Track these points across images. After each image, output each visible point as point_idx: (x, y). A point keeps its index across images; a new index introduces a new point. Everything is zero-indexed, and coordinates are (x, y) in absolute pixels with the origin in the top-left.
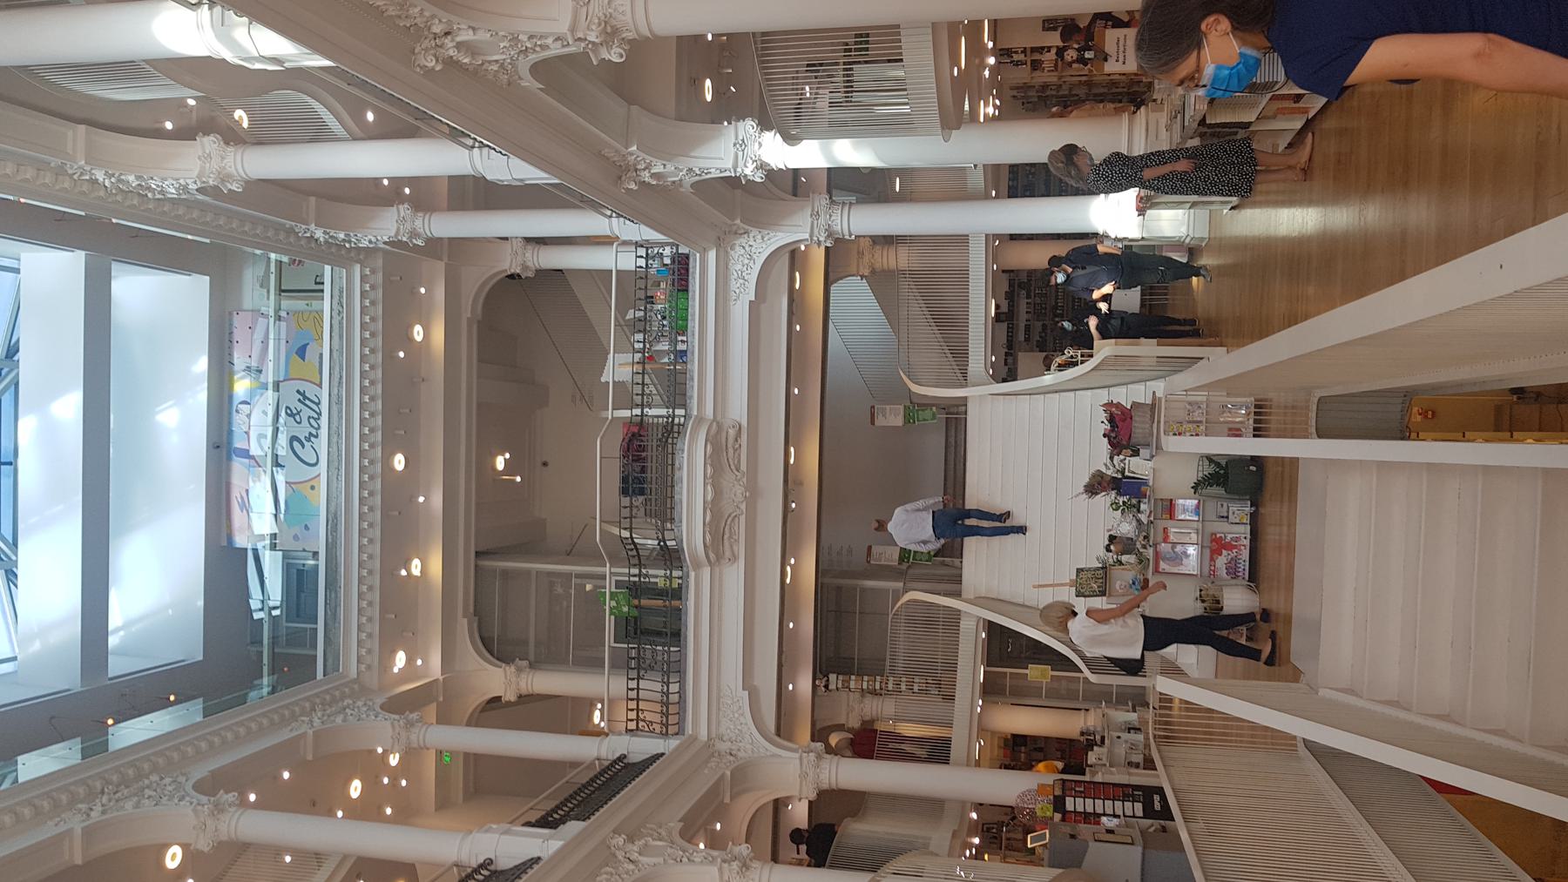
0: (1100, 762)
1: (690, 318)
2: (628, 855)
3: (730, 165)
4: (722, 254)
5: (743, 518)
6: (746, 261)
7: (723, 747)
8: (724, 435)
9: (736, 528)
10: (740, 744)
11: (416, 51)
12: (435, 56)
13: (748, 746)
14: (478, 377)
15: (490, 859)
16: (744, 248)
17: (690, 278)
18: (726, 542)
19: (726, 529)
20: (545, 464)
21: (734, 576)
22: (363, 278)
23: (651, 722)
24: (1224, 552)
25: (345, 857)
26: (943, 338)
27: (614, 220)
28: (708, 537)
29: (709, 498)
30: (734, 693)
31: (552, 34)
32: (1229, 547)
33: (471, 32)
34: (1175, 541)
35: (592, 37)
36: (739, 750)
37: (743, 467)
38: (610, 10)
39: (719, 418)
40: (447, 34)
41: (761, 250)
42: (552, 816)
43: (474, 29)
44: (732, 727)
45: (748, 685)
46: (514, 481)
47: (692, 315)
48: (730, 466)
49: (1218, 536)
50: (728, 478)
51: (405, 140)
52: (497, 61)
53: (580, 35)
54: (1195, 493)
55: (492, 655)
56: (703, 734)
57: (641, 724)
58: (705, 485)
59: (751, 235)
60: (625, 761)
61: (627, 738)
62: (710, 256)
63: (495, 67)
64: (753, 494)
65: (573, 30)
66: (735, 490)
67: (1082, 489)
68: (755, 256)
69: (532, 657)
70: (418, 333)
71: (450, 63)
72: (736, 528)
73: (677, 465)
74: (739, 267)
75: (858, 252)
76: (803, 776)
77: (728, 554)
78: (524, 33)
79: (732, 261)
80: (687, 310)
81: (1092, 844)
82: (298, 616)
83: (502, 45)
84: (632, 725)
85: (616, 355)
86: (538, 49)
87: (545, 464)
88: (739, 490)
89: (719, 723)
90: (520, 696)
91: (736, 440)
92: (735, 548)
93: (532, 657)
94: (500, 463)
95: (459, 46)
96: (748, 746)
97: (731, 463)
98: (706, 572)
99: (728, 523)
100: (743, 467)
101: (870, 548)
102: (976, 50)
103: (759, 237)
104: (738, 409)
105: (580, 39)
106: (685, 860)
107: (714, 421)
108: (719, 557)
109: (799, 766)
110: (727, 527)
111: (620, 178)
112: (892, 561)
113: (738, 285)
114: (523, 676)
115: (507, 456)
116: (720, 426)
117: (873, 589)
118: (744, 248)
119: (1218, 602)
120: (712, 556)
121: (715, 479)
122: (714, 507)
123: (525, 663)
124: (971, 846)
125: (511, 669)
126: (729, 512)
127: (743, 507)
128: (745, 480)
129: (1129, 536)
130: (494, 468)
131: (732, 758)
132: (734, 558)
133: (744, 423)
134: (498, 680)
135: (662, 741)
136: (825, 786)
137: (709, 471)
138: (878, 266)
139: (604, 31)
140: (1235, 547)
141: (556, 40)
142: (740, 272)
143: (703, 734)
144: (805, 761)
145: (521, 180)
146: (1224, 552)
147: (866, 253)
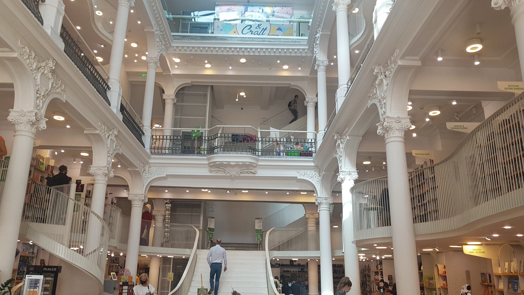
1: (291, 157)
2: (111, 135)
3: (343, 170)
4: (313, 167)
5: (224, 175)
8: (252, 168)
10: (147, 174)
11: (380, 66)
12: (378, 72)
13: (147, 176)
14: (271, 87)
16: (315, 175)
17: (305, 157)
18: (217, 169)
20: (242, 109)
21: (205, 172)
22: (304, 49)
23: (155, 143)
25: (112, 41)
27: (324, 132)
28: (218, 163)
29: (231, 163)
30: (165, 172)
31: (386, 110)
33: (386, 84)
35: (385, 124)
36: (146, 173)
37: (241, 175)
38: (394, 129)
39: (258, 166)
40: (386, 76)
43: (387, 85)
44: (153, 171)
45: (168, 176)
46: (237, 99)
50: (238, 170)
52: (377, 92)
53: (386, 120)
55: (178, 91)
57: (155, 140)
59: (319, 177)
61: (150, 135)
63: (375, 92)
64: (233, 178)
65: (387, 117)
66: (234, 172)
67: (235, 290)
68: (312, 178)
69: (177, 104)
70: (286, 67)
71: (376, 77)
72: (221, 172)
73: (242, 152)
75: (313, 213)
76: (136, 195)
77: (212, 169)
78: (386, 101)
79: (310, 171)
82: (192, 27)
83: (382, 94)
84: (154, 137)
86: (381, 106)
87: (242, 109)
88: (234, 173)
90: (164, 100)
91: (251, 172)
92: (214, 172)
93: (177, 104)
94: (242, 94)
95: (382, 80)
96: (147, 176)
97: (243, 171)
98: (206, 162)
99: (223, 170)
100: (241, 175)
101: (214, 218)
102: (382, 252)
103: (318, 180)
104: (261, 173)
105: (384, 119)
107: (257, 165)
108: (211, 167)
110: (221, 169)
111: (338, 133)
112: (209, 226)
113: (302, 173)
114: (171, 101)
115: (245, 96)
116: (255, 167)
117: (200, 218)
118: (315, 175)
120: (212, 164)
121: (237, 165)
122: (228, 165)
123: (176, 102)
124: (111, 253)
125: (174, 97)
126: (227, 170)
127: (228, 175)
128: (237, 175)
130: (241, 92)
131: (143, 171)
132: (211, 172)
133: (256, 175)
134: (170, 93)
135: (149, 147)
136: (133, 203)
137: (240, 163)
138: (309, 220)
139: (387, 128)
141: (384, 112)
142: (307, 173)
144: (142, 196)
145: (337, 101)
147: (313, 216)
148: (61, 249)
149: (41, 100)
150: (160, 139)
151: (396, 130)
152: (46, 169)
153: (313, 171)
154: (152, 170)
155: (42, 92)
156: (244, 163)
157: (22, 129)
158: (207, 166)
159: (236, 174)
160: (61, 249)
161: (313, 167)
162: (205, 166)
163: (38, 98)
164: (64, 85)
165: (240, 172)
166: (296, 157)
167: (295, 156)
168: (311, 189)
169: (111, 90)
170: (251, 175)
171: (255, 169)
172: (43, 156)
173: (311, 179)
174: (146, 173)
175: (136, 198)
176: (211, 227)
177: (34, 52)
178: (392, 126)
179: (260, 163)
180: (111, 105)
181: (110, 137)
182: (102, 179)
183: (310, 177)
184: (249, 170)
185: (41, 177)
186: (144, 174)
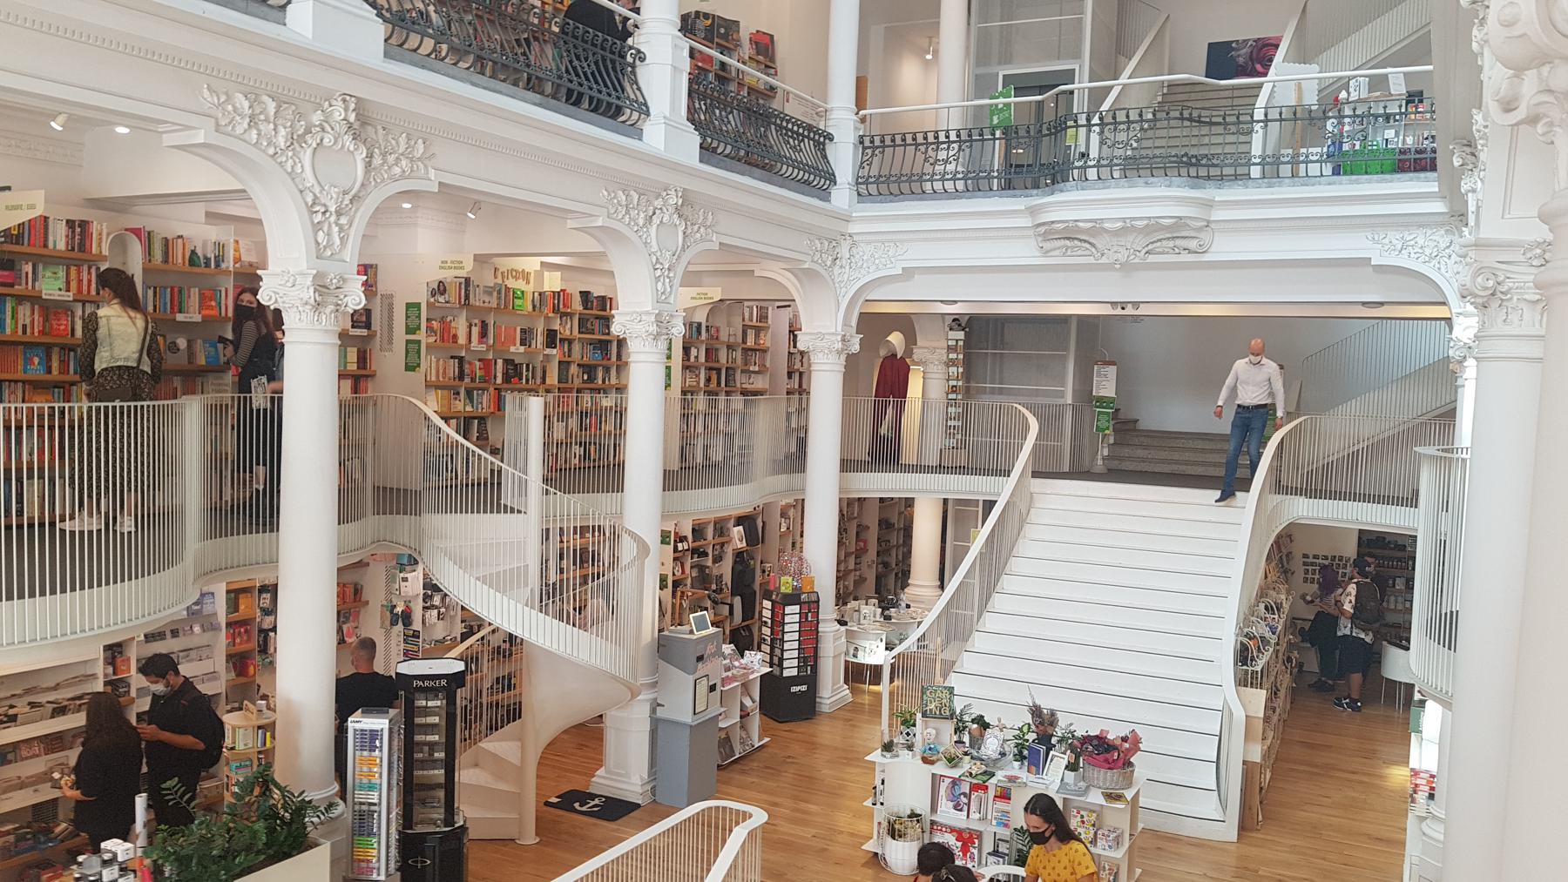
0: (862, 617)
1: (1354, 177)
2: (658, 212)
4: (1440, 219)
5: (1091, 260)
6: (1428, 251)
7: (844, 251)
9: (1079, 253)
10: (848, 267)
13: (846, 276)
15: (645, 59)
16: (1448, 247)
17: (1411, 175)
18: (1062, 242)
19: (1076, 242)
24: (959, 844)
26: (1358, 450)
28: (1061, 226)
30: (899, 258)
32: (965, 850)
34: (973, 797)
36: (841, 267)
37: (1152, 258)
38: (1515, 298)
41: (1443, 270)
42: (719, 97)
44: (865, 258)
45: (908, 273)
47: (1357, 180)
48: (1152, 243)
49: (976, 841)
50: (1140, 242)
51: (661, 450)
54: (1015, 829)
56: (853, 228)
58: (1124, 220)
60: (827, 141)
62: (1439, 204)
67: (1038, 702)
72: (1079, 253)
74: (1421, 241)
76: (821, 336)
77: (1047, 245)
79: (1429, 232)
80: (1366, 173)
81: (691, 678)
85: (1317, 81)
89: (869, 243)
96: (846, 276)
97: (1155, 245)
99: (1084, 245)
104: (1225, 248)
106: (658, 273)
109: (829, 331)
110: (1079, 244)
112: (1098, 387)
113: (1394, 242)
117: (1065, 367)
118: (1448, 247)
119: (900, 837)
120: (1042, 229)
122: (1097, 228)
126: (1098, 245)
127: (1104, 260)
128: (1137, 261)
129: (983, 748)
133: (1207, 258)
137: (1138, 223)
140: (965, 855)
142: (1413, 242)
143: (853, 228)
144: (834, 338)
146: (959, 844)
148: (492, 600)
149: (334, 225)
150: (884, 147)
151: (1523, 305)
152: (534, 307)
153: (1443, 232)
154: (861, 254)
155: (328, 204)
156: (1153, 221)
157: (295, 326)
158: (1031, 232)
159: (1132, 257)
160: (492, 600)
161: (1440, 219)
162: (1025, 233)
163: (317, 227)
164: (420, 141)
165: (1144, 251)
166: (1375, 177)
167: (1370, 174)
168: (1442, 300)
169: (647, 62)
170: (1186, 257)
171: (1201, 235)
172: (523, 270)
173: (1431, 265)
174: (841, 267)
175: (819, 343)
176: (1103, 393)
177: (269, 96)
178: (1508, 284)
179: (1218, 215)
180: (652, 117)
181: (656, 220)
182: (647, 349)
183: (1427, 259)
184: (1179, 242)
185: (523, 331)
186: (837, 270)
